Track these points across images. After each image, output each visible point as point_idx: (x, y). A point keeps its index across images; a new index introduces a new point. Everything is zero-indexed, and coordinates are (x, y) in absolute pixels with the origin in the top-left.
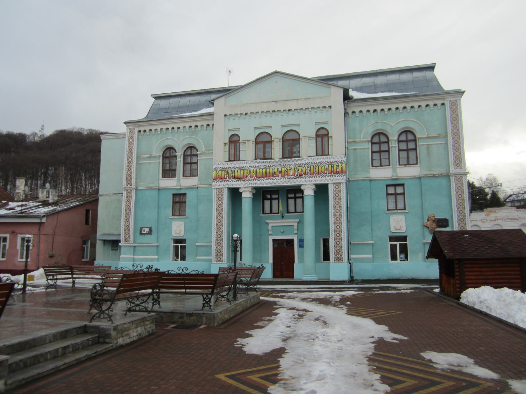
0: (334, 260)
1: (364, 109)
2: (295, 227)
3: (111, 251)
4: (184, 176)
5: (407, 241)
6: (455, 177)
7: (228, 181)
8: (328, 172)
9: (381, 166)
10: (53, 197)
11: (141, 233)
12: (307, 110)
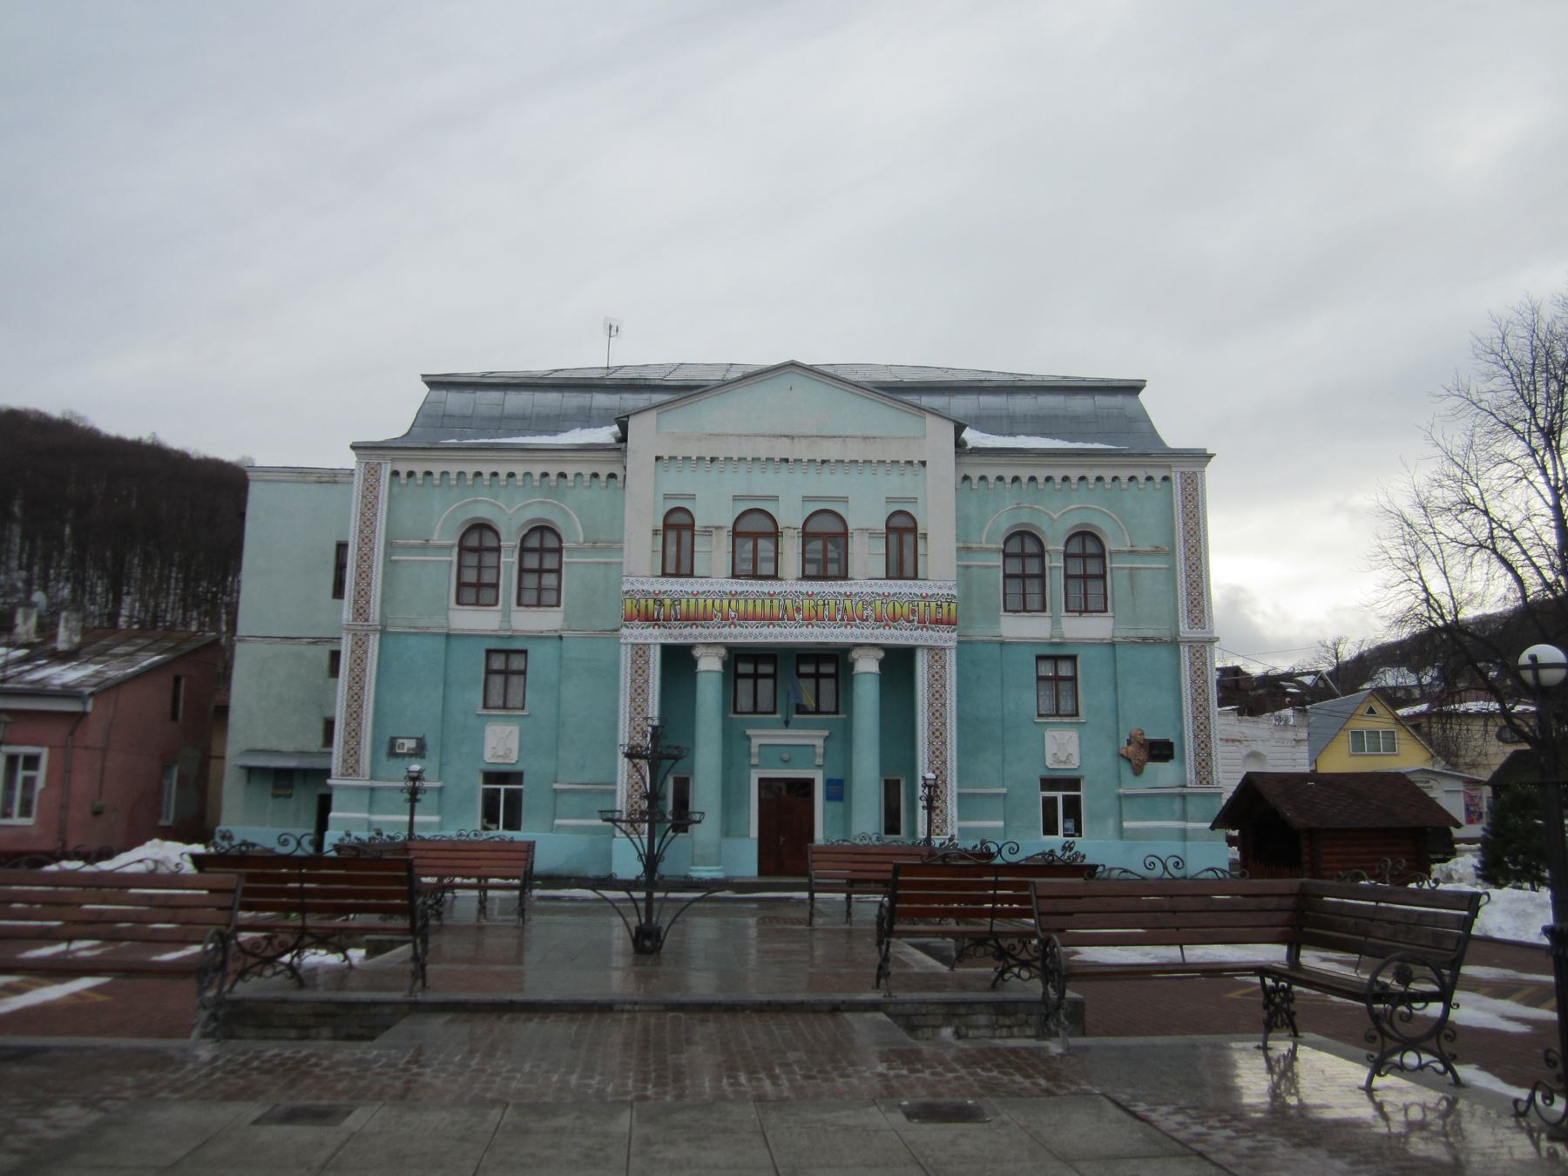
1: (992, 473)
2: (820, 750)
4: (519, 604)
5: (1079, 790)
6: (1190, 646)
8: (916, 618)
9: (1025, 610)
10: (70, 637)
11: (393, 753)
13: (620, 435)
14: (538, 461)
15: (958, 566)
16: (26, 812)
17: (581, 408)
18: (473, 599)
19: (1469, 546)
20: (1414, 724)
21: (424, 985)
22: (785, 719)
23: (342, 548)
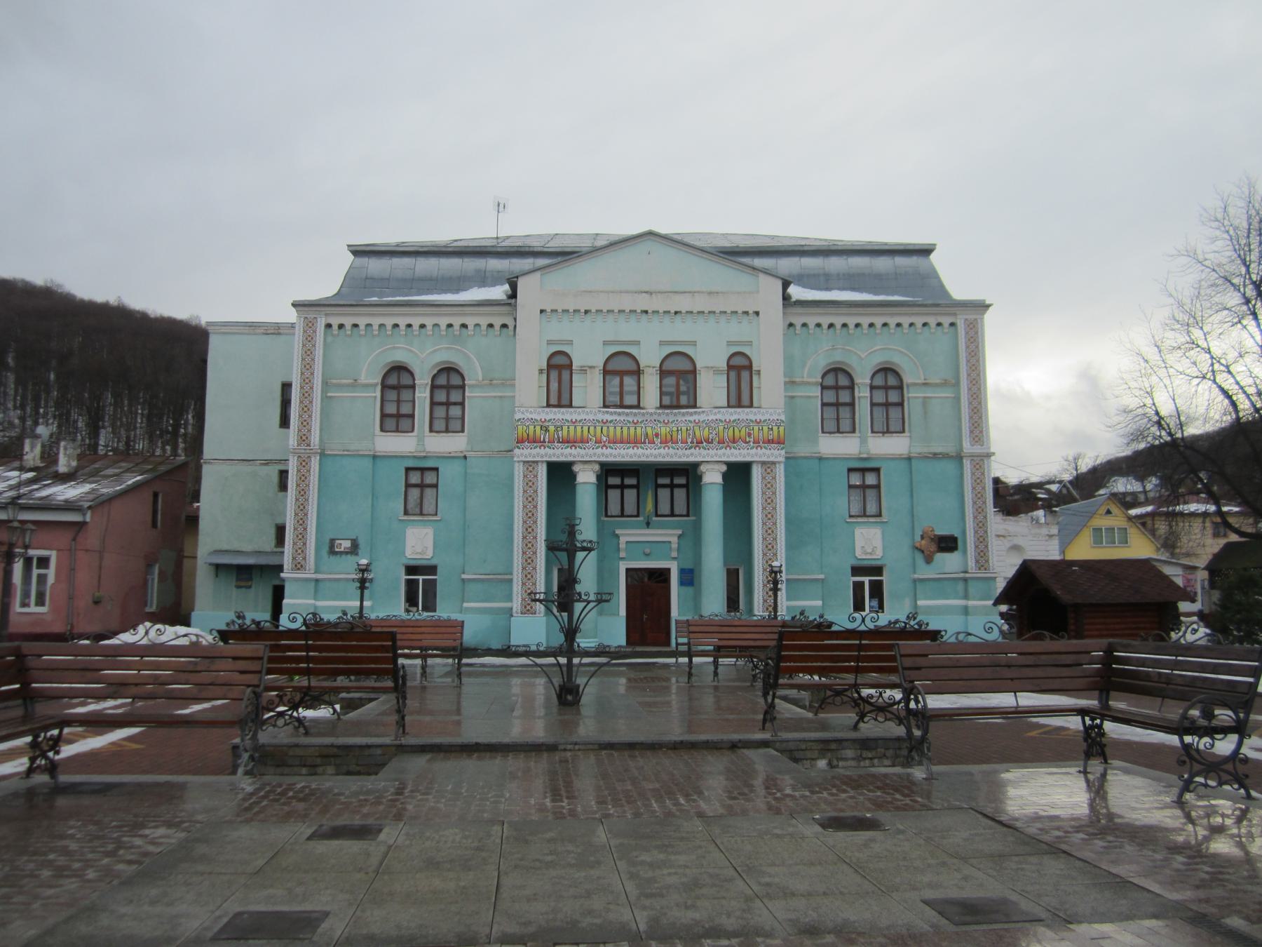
0: (761, 610)
1: (812, 322)
2: (675, 546)
3: (234, 589)
4: (431, 431)
5: (881, 575)
7: (548, 447)
8: (752, 440)
9: (838, 432)
10: (68, 461)
11: (332, 552)
12: (712, 315)
13: (510, 292)
14: (445, 315)
15: (785, 396)
16: (40, 601)
17: (478, 271)
18: (394, 428)
19: (1194, 377)
20: (1142, 521)
21: (404, 732)
22: (646, 521)
23: (286, 387)
